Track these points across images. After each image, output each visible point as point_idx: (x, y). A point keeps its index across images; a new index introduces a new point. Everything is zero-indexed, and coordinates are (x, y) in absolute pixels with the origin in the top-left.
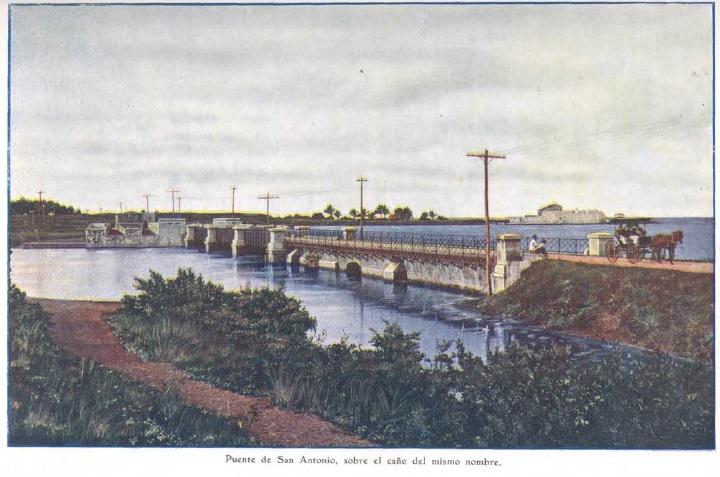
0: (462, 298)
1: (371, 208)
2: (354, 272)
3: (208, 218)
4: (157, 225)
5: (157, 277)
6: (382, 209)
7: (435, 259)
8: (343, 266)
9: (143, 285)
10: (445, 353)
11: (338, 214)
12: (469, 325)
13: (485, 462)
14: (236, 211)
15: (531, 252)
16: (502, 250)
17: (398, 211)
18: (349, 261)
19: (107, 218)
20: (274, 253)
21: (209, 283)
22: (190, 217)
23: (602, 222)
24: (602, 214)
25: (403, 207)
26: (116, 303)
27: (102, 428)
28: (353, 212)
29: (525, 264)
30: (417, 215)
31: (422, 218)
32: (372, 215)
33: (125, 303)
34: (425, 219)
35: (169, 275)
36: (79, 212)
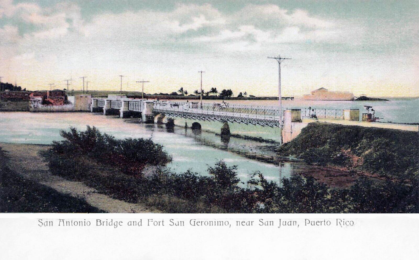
0: (264, 144)
1: (207, 89)
2: (196, 127)
3: (105, 95)
4: (73, 97)
5: (74, 130)
6: (214, 90)
7: (250, 121)
8: (190, 125)
9: (64, 134)
10: (253, 178)
11: (186, 93)
12: (268, 161)
13: (79, 223)
14: (123, 90)
15: (355, 100)
16: (289, 117)
17: (224, 91)
18: (194, 121)
19: (43, 94)
20: (147, 116)
21: (199, 17)
22: (93, 94)
23: (353, 100)
24: (352, 94)
25: (223, 90)
26: (48, 145)
27: (58, 92)
28: (196, 92)
29: (304, 125)
30: (235, 95)
31: (239, 96)
32: (208, 93)
33: (53, 145)
34: (240, 97)
35: (82, 128)
36: (25, 90)
